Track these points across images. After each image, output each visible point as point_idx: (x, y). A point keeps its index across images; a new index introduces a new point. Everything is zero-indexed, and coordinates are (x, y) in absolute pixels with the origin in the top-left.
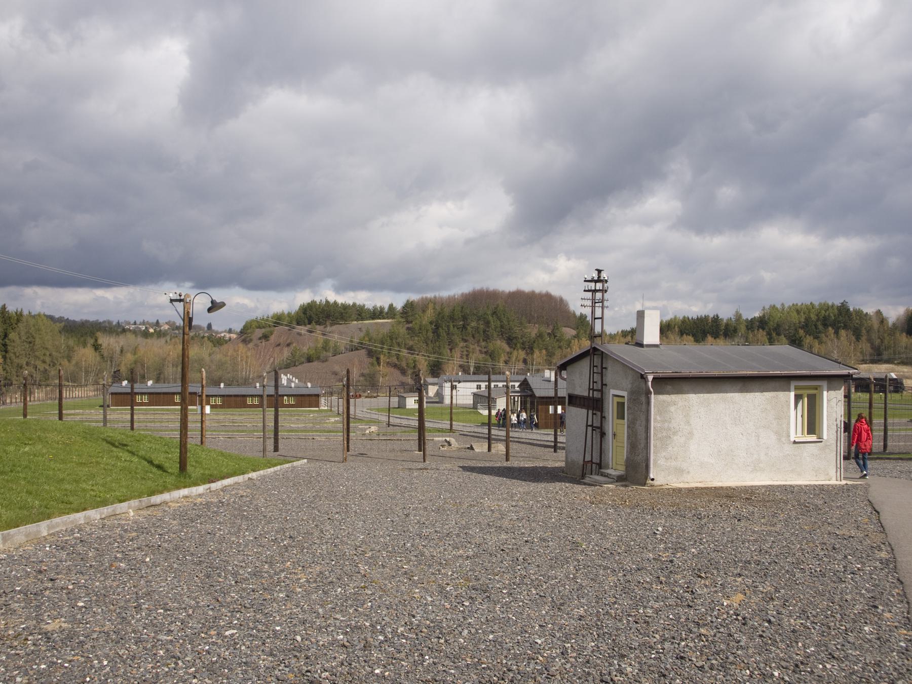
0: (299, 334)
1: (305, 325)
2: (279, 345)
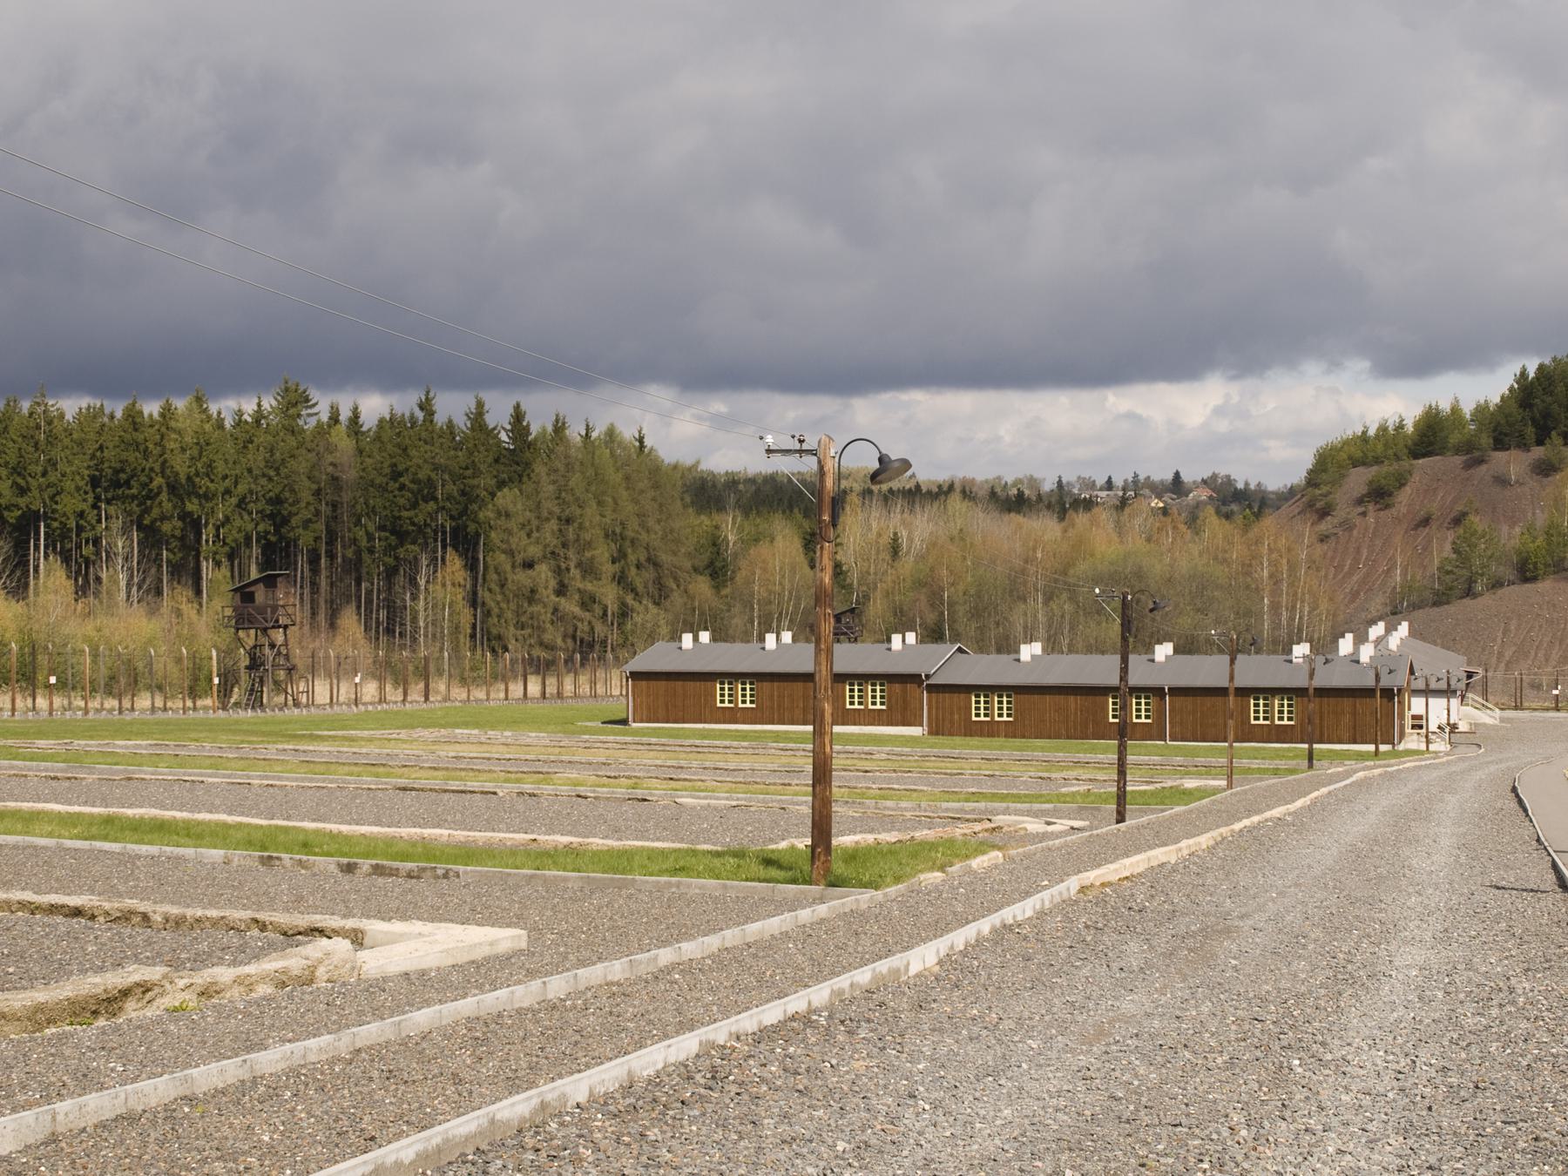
0: (1502, 481)
1: (1524, 446)
2: (1426, 522)
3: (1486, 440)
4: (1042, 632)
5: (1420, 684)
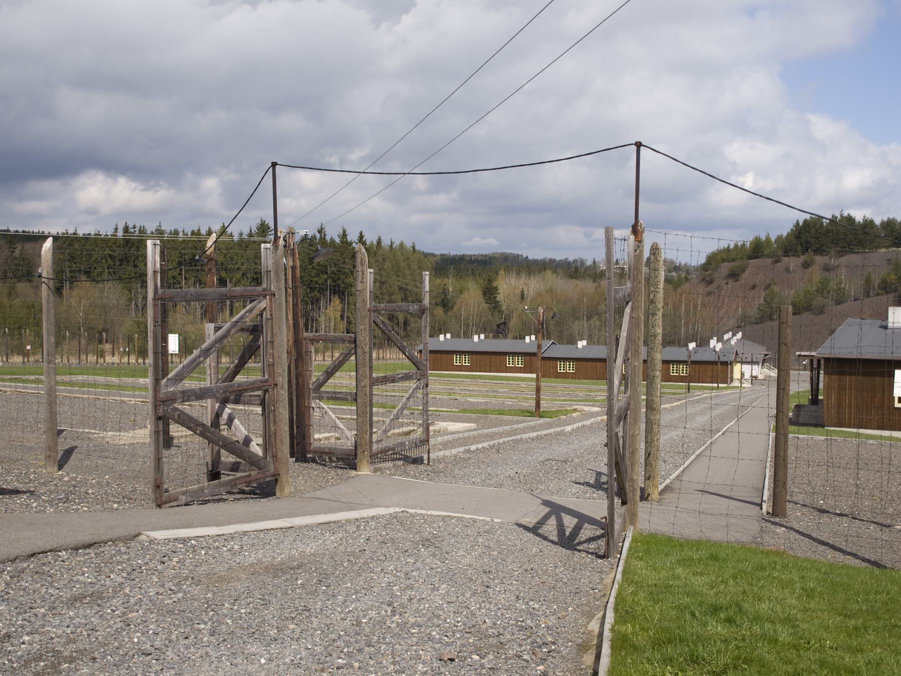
2: (754, 287)
3: (780, 253)
4: (586, 334)
5: (739, 359)
